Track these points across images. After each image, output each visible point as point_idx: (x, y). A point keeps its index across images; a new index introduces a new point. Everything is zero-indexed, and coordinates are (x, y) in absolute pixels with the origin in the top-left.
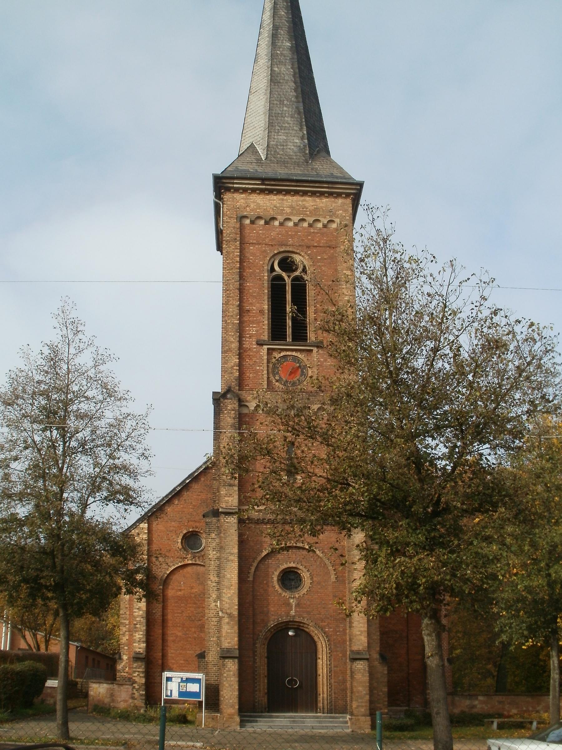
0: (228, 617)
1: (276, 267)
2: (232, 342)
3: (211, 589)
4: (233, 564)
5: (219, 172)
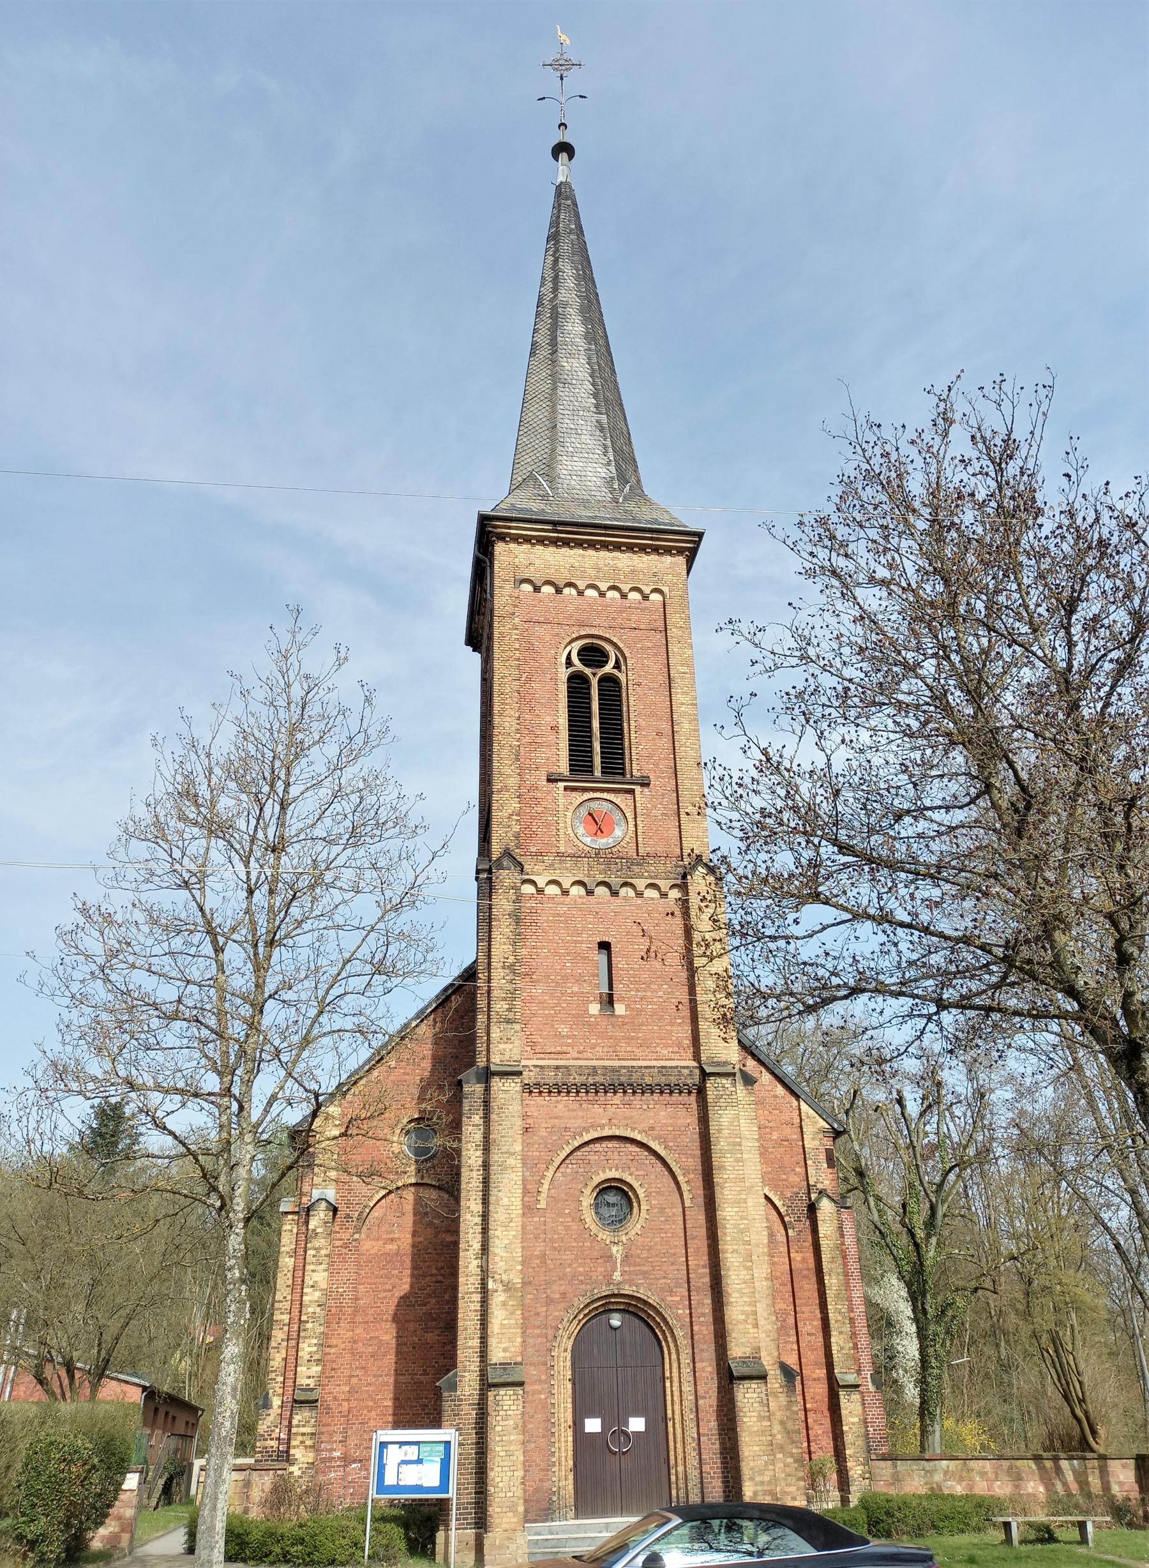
0: (505, 1291)
1: (575, 659)
2: (510, 776)
3: (471, 1231)
4: (513, 1176)
5: (487, 509)
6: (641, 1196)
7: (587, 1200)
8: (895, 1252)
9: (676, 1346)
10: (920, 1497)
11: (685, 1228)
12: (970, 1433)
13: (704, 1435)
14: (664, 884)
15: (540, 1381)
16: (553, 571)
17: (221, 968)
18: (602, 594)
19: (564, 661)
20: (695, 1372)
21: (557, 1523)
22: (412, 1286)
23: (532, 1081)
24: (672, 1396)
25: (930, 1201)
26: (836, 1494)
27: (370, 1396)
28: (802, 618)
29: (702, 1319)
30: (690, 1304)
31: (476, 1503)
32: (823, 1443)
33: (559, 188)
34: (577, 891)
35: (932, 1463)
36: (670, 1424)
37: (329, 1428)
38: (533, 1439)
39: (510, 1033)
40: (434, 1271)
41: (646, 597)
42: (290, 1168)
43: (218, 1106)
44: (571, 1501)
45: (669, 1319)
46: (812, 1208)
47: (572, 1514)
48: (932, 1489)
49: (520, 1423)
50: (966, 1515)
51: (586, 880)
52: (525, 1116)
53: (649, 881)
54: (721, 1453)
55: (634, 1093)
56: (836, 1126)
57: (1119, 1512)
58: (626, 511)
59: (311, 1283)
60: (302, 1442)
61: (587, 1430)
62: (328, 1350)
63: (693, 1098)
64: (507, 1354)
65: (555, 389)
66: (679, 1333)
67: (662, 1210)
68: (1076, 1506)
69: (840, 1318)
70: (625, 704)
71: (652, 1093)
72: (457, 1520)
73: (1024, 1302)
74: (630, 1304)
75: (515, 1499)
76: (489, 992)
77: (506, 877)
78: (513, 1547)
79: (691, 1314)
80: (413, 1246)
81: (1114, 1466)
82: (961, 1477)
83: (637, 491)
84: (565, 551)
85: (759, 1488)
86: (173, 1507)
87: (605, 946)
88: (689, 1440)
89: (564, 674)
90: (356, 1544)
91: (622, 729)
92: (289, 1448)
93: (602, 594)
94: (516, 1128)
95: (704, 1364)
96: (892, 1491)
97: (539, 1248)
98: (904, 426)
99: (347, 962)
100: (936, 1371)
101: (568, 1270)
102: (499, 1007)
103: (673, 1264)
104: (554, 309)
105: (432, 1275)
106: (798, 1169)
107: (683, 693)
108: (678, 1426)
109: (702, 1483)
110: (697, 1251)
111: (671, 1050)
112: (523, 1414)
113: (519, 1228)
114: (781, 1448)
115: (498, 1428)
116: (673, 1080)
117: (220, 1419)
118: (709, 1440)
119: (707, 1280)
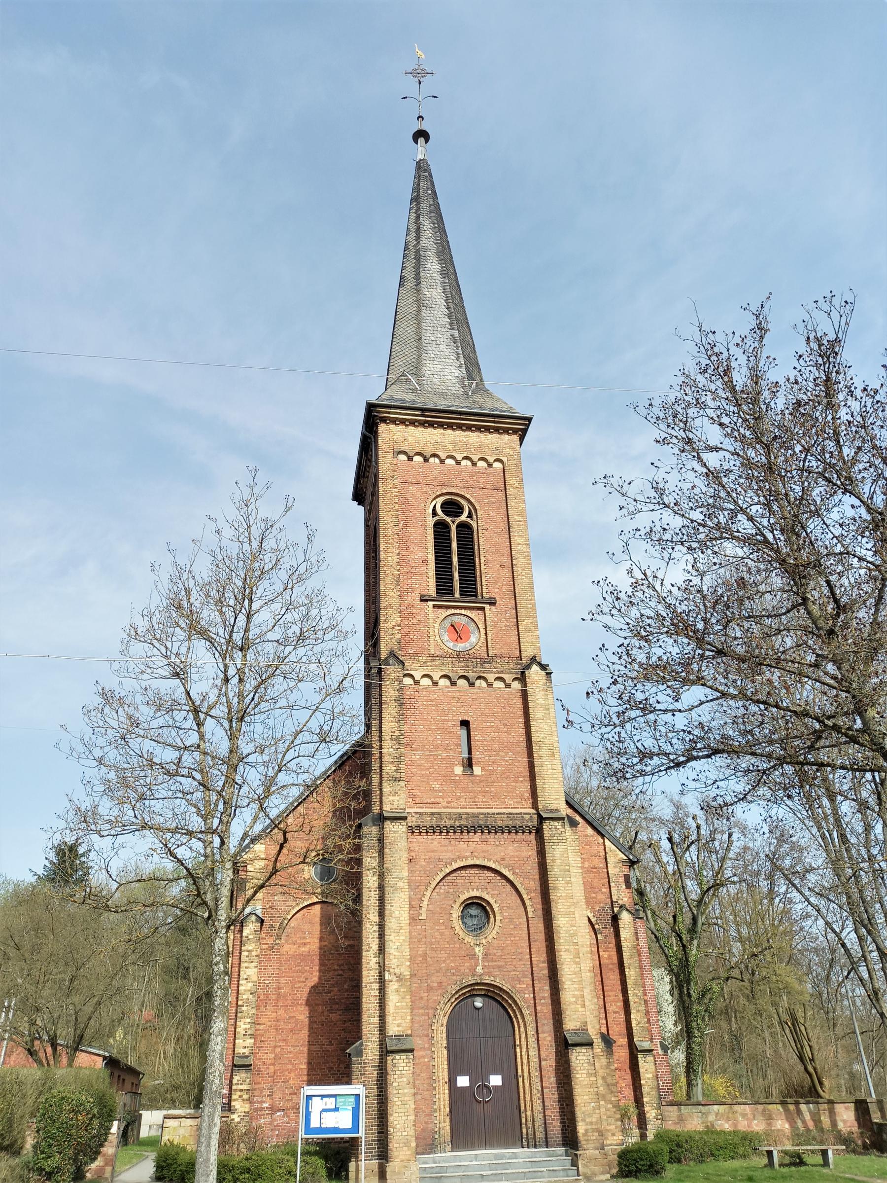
1: (439, 510)
2: (392, 597)
3: (371, 936)
4: (402, 895)
5: (373, 399)
6: (496, 909)
7: (456, 912)
8: (667, 952)
9: (524, 1021)
10: (699, 1132)
11: (529, 933)
12: (719, 1085)
13: (546, 1088)
14: (508, 678)
15: (424, 1048)
16: (422, 445)
17: (202, 737)
18: (458, 463)
19: (431, 511)
20: (538, 1040)
21: (439, 1155)
22: (320, 978)
23: (414, 824)
24: (522, 1059)
25: (693, 913)
26: (636, 1131)
27: (290, 1061)
28: (660, 476)
29: (543, 1001)
30: (534, 990)
31: (378, 1140)
32: (626, 1093)
33: (418, 163)
34: (444, 682)
35: (707, 1107)
36: (520, 1080)
37: (260, 1086)
38: (420, 1092)
39: (397, 788)
40: (336, 967)
41: (490, 465)
42: (262, 887)
43: (204, 841)
44: (448, 1138)
45: (518, 1001)
46: (615, 919)
47: (449, 1148)
48: (707, 1127)
49: (411, 1080)
50: (735, 1146)
51: (450, 675)
52: (410, 850)
53: (497, 675)
54: (559, 1101)
55: (489, 832)
56: (631, 857)
57: (845, 1140)
58: (474, 402)
59: (245, 977)
60: (240, 1096)
61: (459, 1085)
62: (258, 1027)
63: (533, 836)
64: (401, 1028)
65: (419, 311)
66: (526, 1012)
67: (511, 920)
68: (814, 1139)
69: (637, 1000)
70: (476, 544)
71: (503, 832)
72: (366, 1153)
73: (749, 988)
74: (489, 991)
75: (409, 1137)
76: (381, 757)
77: (392, 671)
78: (408, 1173)
79: (534, 997)
80: (320, 948)
81: (839, 1108)
82: (728, 1117)
83: (481, 388)
84: (430, 430)
85: (589, 1127)
86: (129, 1147)
87: (465, 724)
88: (535, 1091)
89: (431, 521)
90: (290, 1173)
91: (474, 563)
92: (230, 1101)
93: (458, 463)
94: (403, 859)
95: (545, 1035)
96: (678, 1129)
97: (422, 949)
98: (734, 333)
99: (297, 734)
100: (698, 1040)
101: (443, 965)
102: (389, 768)
103: (520, 960)
104: (417, 252)
105: (334, 970)
106: (604, 890)
107: (519, 536)
108: (526, 1081)
109: (545, 1123)
110: (538, 951)
111: (515, 800)
112: (413, 1073)
113: (407, 934)
114: (604, 1097)
115: (395, 1084)
116: (518, 823)
117: (211, 1078)
118: (550, 1091)
119: (546, 972)
